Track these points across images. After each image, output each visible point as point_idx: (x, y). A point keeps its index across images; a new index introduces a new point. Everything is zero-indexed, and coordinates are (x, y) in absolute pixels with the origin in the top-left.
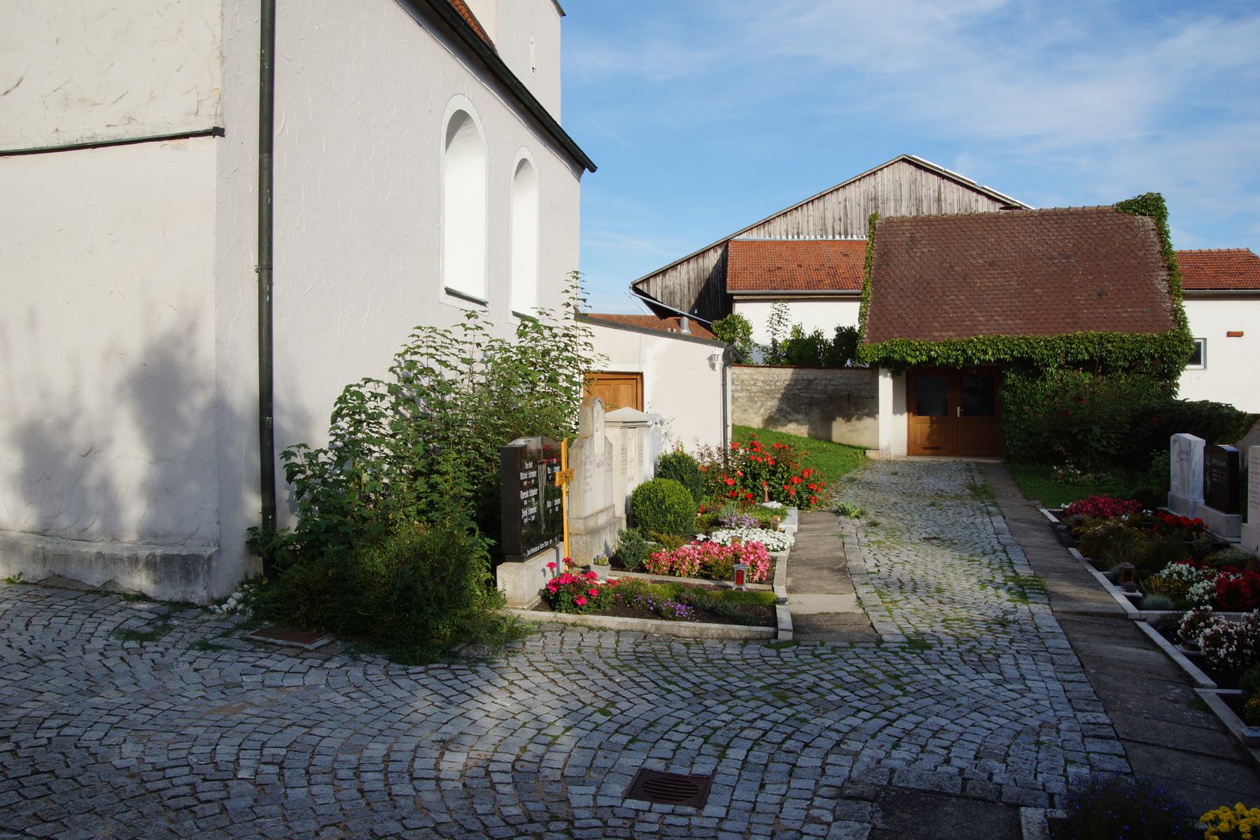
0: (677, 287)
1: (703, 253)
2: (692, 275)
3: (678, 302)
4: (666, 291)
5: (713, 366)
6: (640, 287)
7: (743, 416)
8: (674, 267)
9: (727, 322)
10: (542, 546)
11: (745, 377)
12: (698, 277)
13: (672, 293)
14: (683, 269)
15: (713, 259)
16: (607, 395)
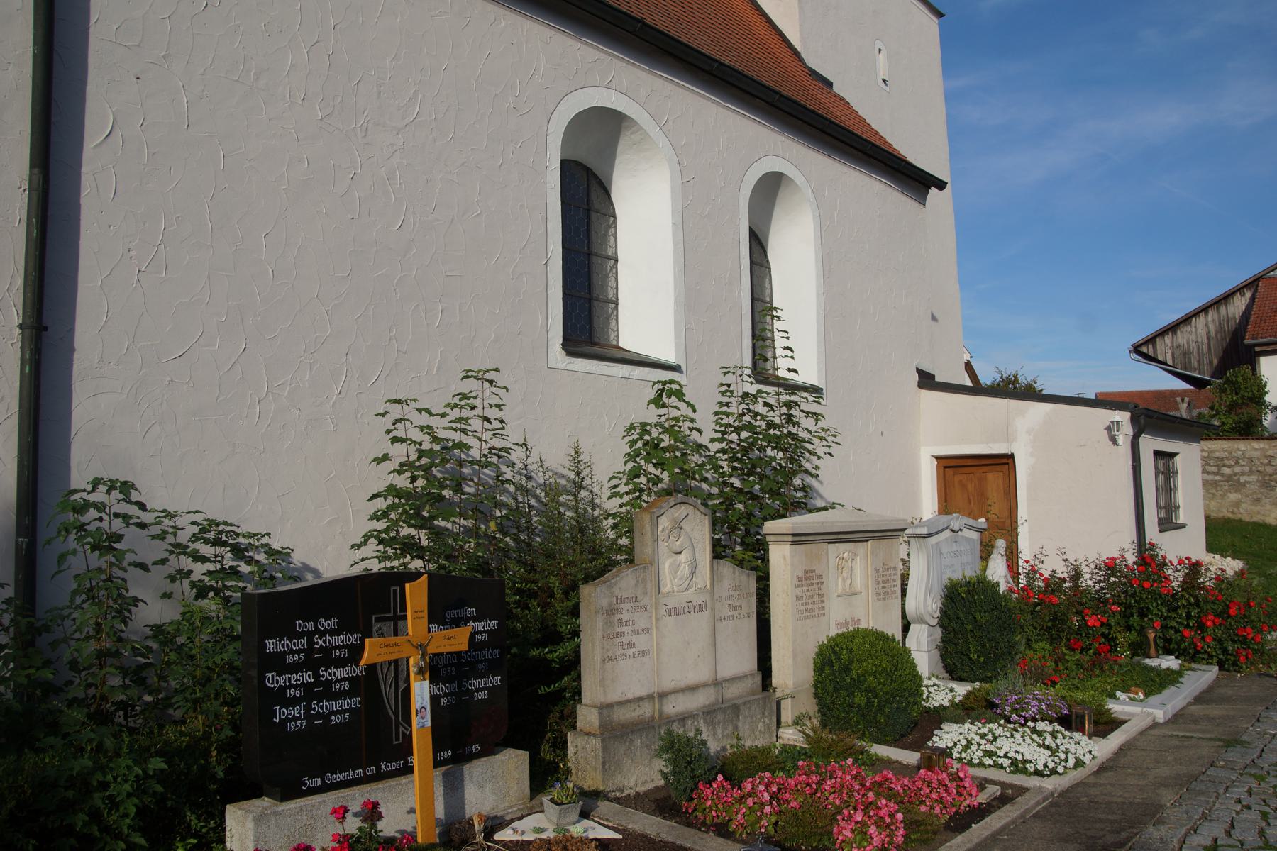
0: (1193, 345)
1: (1226, 298)
2: (1212, 328)
3: (1195, 364)
4: (1178, 352)
5: (1114, 440)
6: (1144, 349)
7: (1255, 509)
8: (1186, 320)
9: (1227, 382)
10: (350, 775)
11: (1255, 454)
12: (1220, 329)
13: (1186, 354)
14: (1200, 322)
15: (1238, 305)
16: (970, 487)
